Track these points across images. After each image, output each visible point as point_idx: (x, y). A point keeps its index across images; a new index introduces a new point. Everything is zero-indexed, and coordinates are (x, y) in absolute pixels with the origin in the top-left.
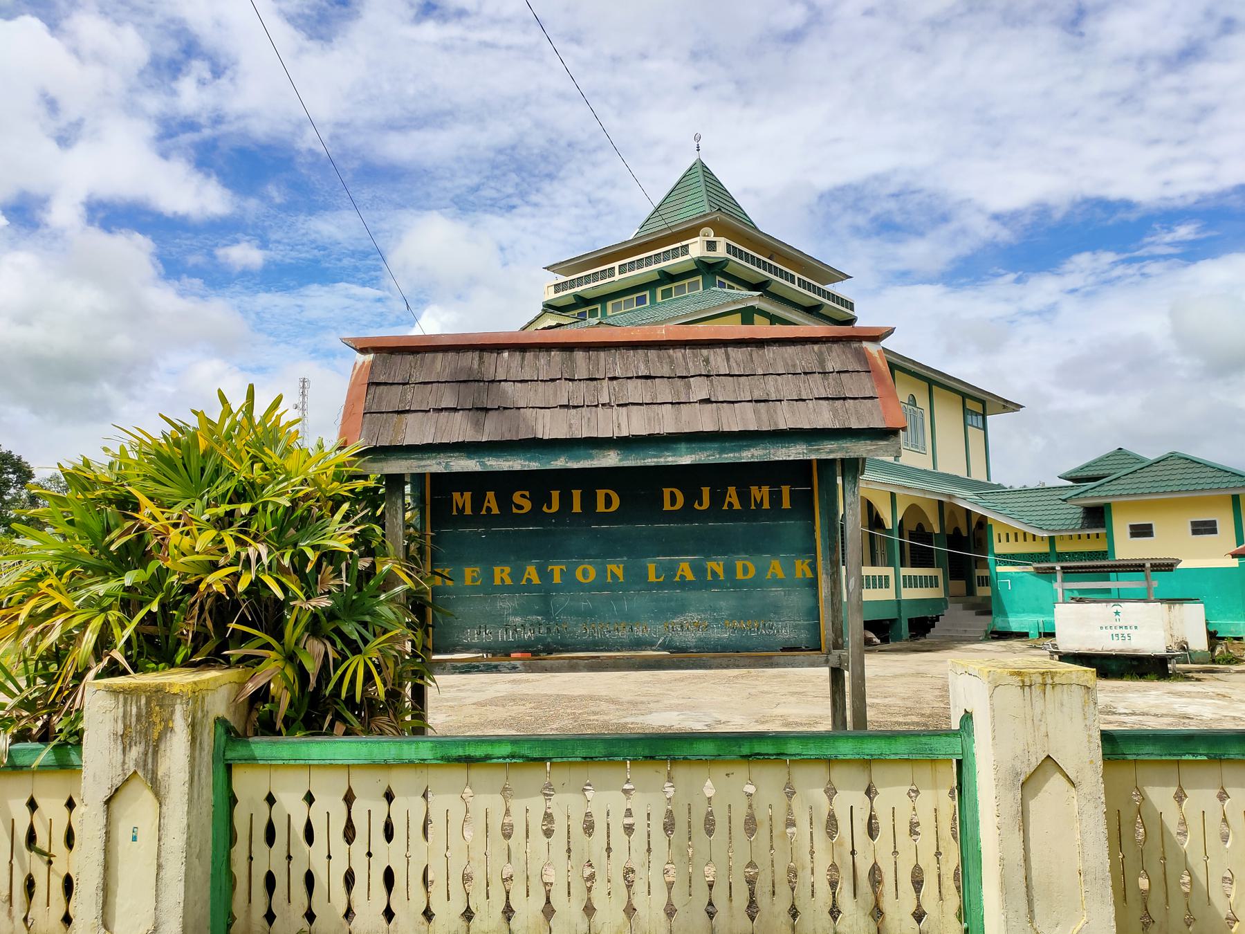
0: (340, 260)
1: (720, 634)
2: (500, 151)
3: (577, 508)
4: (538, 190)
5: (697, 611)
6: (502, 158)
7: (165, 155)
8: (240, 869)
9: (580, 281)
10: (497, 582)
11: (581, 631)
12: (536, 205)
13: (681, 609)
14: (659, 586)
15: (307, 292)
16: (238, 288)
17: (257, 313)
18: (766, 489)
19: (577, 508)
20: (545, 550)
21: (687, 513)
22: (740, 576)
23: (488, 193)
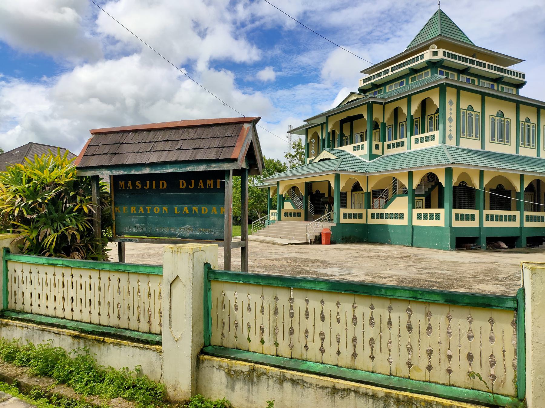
0: (310, 73)
1: (197, 233)
2: (382, 13)
3: (154, 187)
4: (401, 29)
5: (190, 224)
6: (383, 16)
7: (236, 38)
8: (9, 289)
9: (374, 77)
10: (132, 212)
11: (156, 230)
12: (399, 36)
13: (184, 224)
14: (177, 215)
15: (297, 88)
16: (270, 89)
17: (277, 99)
18: (212, 181)
19: (154, 187)
20: (146, 202)
21: (187, 190)
22: (203, 212)
23: (376, 34)
